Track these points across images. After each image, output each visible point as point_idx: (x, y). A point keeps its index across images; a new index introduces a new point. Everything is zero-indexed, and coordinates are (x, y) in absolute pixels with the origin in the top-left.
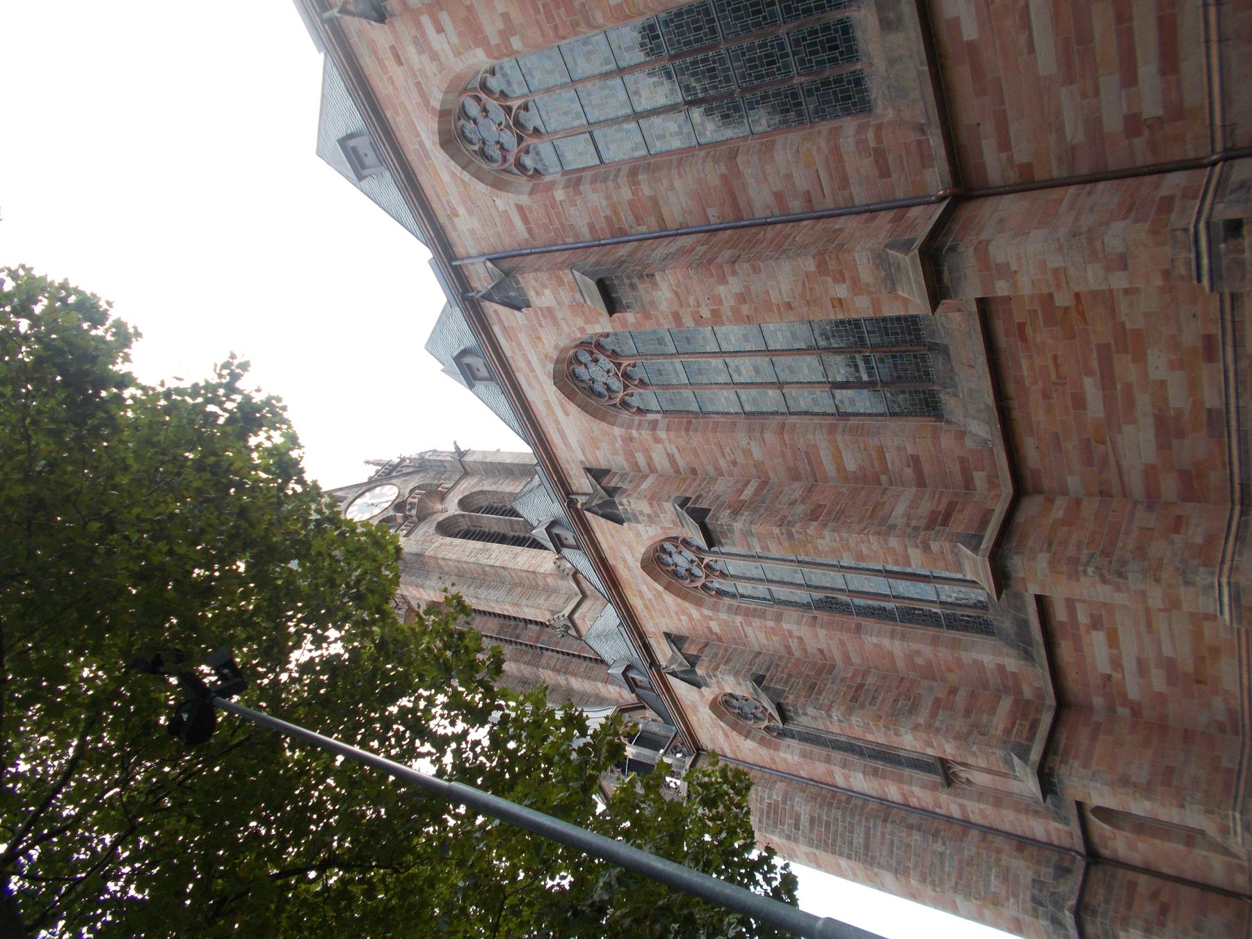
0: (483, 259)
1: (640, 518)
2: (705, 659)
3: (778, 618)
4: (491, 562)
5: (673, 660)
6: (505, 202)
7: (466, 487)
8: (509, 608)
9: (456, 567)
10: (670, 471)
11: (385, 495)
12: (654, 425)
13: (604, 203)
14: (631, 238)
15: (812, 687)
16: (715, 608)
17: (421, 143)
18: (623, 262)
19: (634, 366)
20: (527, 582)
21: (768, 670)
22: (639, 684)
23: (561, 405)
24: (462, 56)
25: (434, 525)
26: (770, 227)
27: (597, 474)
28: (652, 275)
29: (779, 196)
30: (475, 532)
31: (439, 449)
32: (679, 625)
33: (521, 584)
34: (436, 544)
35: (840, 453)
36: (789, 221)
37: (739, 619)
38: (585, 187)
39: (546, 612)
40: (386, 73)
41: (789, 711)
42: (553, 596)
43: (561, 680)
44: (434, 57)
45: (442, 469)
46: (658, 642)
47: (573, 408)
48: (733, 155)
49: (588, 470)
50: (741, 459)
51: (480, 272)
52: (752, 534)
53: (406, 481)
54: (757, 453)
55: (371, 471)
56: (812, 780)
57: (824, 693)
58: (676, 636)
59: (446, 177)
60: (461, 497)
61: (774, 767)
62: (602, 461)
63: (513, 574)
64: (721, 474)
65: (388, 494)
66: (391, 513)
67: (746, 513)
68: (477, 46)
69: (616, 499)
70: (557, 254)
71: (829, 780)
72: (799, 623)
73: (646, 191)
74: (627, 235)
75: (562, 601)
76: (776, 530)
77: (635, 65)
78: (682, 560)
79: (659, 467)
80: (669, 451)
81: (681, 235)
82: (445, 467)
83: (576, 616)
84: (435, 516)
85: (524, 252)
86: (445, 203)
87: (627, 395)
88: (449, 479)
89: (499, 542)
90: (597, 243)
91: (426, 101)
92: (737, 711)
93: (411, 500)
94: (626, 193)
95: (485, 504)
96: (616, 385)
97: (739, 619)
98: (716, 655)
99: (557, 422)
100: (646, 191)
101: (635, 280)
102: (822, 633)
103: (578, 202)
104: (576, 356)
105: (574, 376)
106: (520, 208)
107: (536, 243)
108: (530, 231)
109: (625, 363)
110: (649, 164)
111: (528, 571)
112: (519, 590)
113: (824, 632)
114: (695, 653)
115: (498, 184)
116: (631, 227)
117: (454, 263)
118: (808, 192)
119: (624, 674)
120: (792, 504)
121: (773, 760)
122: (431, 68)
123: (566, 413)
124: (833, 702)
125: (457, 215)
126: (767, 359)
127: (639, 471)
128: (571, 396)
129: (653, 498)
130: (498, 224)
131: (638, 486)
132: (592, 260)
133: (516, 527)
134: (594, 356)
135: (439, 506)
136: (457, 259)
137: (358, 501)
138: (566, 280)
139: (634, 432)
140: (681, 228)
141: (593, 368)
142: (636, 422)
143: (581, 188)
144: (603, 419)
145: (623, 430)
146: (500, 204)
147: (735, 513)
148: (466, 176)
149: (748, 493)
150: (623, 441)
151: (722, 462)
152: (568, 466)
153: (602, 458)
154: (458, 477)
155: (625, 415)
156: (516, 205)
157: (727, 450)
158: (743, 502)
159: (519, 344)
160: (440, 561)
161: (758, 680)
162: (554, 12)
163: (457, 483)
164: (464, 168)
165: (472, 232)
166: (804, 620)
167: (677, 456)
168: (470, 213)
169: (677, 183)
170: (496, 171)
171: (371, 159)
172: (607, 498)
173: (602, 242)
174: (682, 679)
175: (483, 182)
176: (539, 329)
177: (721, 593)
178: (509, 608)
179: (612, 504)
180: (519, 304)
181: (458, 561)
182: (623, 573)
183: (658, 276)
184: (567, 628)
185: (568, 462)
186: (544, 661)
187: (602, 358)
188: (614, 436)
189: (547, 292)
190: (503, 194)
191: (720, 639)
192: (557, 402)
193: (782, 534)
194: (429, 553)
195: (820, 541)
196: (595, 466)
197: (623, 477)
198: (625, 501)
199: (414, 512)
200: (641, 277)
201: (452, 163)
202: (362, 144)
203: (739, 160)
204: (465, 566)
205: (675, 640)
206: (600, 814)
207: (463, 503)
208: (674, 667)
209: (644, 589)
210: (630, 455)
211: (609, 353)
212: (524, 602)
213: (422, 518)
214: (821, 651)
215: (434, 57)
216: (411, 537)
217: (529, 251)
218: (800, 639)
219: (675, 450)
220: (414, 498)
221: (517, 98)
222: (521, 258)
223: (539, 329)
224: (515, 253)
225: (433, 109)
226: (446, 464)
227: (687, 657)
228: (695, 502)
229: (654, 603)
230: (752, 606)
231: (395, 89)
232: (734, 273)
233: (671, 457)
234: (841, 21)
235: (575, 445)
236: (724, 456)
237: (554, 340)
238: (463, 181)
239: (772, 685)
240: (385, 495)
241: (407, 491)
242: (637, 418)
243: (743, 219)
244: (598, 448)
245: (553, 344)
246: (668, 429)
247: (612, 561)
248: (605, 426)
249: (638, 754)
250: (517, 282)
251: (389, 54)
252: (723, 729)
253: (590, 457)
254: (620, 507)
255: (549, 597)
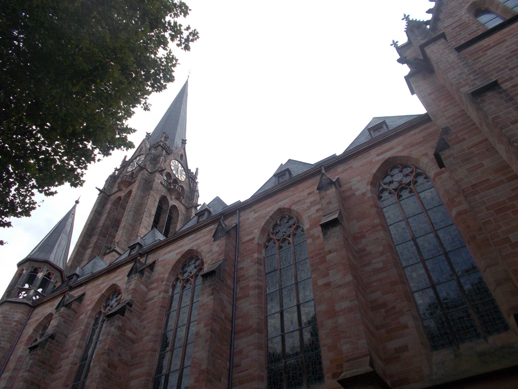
0: (237, 223)
1: (128, 285)
2: (69, 312)
3: (79, 347)
4: (144, 218)
5: (72, 296)
6: (257, 232)
7: (181, 208)
8: (123, 224)
9: (145, 203)
10: (147, 299)
11: (181, 176)
12: (166, 291)
13: (250, 274)
14: (235, 285)
15: (44, 363)
16: (90, 316)
17: (281, 201)
18: (222, 281)
19: (191, 284)
20: (134, 232)
21: (57, 341)
22: (70, 280)
23: (181, 252)
24: (308, 219)
25: (165, 195)
26: (229, 347)
27: (152, 266)
28: (213, 294)
29: (241, 352)
30: (161, 211)
31: (199, 198)
32: (87, 298)
33: (133, 230)
34: (155, 195)
35: (138, 378)
36: (230, 356)
37: (83, 328)
38: (256, 267)
39: (118, 240)
40: (306, 189)
41: (34, 351)
42: (126, 243)
43: (92, 245)
44: (309, 208)
45: (190, 199)
46: (82, 290)
47: (179, 256)
48: (259, 331)
49: (154, 262)
50: (145, 331)
51: (234, 221)
52: (108, 335)
53: (187, 184)
54: (146, 338)
55: (193, 171)
56: (8, 361)
57: (39, 368)
58: (83, 298)
59: (268, 209)
60: (177, 206)
61: (18, 343)
62: (157, 268)
63: (138, 226)
64: (141, 322)
65: (182, 177)
66: (173, 178)
67: (118, 333)
68: (310, 225)
69: (137, 274)
70: (234, 253)
71: (6, 370)
72: (75, 356)
73: (252, 292)
74: (237, 283)
75: (123, 246)
76: (107, 347)
77: (298, 290)
78: (191, 269)
79: (150, 293)
80: (155, 298)
81: (233, 307)
82: (191, 200)
83: (114, 253)
84: (169, 195)
85: (237, 240)
86: (260, 209)
87: (180, 280)
88: (186, 201)
89: (154, 221)
90: (236, 270)
91: (295, 203)
92: (47, 326)
93: (177, 186)
94: (252, 284)
95: (173, 216)
96: (185, 275)
97: (83, 328)
98: (70, 316)
99: (175, 250)
100: (252, 292)
101: (212, 287)
102: (68, 368)
103: (252, 263)
104: (198, 259)
105: (192, 258)
106: (253, 239)
107: (240, 244)
108: (245, 242)
109: (192, 280)
110: (262, 294)
111: (138, 233)
112: (131, 229)
113: (68, 369)
114: (72, 307)
115: (263, 230)
116: (240, 285)
117: (238, 211)
118: (240, 366)
119: (75, 274)
120: (119, 355)
121: (21, 342)
122: (305, 206)
123: (177, 254)
124: (33, 373)
125: (255, 213)
126: (182, 345)
127: (150, 284)
128: (184, 256)
129: (135, 290)
130: (249, 230)
131: (142, 283)
132: (227, 268)
133: (161, 228)
134: (197, 267)
135: (173, 197)
136: (239, 212)
137: (180, 165)
138: (220, 257)
139: (165, 283)
140: (235, 307)
141: (193, 266)
142: (169, 284)
143: (257, 265)
144: (172, 269)
145: (166, 278)
146: (256, 231)
147: (119, 328)
148: (268, 218)
149: (129, 334)
150: (163, 278)
151: (146, 322)
152: (157, 254)
153: (158, 268)
154: (186, 205)
155: (173, 279)
156: (255, 237)
157: (150, 325)
158: (125, 332)
159: (205, 235)
160: (148, 196)
161: (52, 337)
162: (318, 257)
163: (184, 205)
164: (271, 217)
165: (248, 219)
166: (76, 359)
167: (152, 301)
168: (255, 219)
169: (252, 306)
170: (269, 230)
171: (281, 180)
172: (139, 270)
173: (236, 273)
174: (61, 301)
175: (265, 224)
176: (210, 244)
177: (174, 287)
178: (123, 224)
179: (136, 272)
180: (215, 237)
181: (146, 204)
182: (112, 275)
183: (212, 297)
184: (110, 249)
185: (159, 254)
186: (101, 238)
187: (195, 270)
188: (165, 274)
189: (217, 249)
190: (259, 232)
191: (77, 318)
192: (182, 250)
193: (105, 350)
194: (152, 192)
195: (98, 368)
196: (156, 265)
197: (149, 278)
198: (136, 278)
199: (172, 187)
200: (213, 289)
201: (273, 212)
202: (287, 176)
203: (257, 334)
204: (144, 207)
205: (81, 298)
206: (310, 238)
207: (174, 207)
208: (67, 297)
209: (104, 285)
210: (156, 281)
211: (197, 273)
212: (125, 231)
213: (169, 190)
214: (61, 367)
215: (309, 208)
216: (161, 185)
217: (237, 241)
218: (68, 357)
219: (155, 300)
220: (178, 187)
221: (293, 240)
222: (235, 238)
223: (210, 244)
224: (238, 236)
225: (291, 206)
226: (192, 201)
227: (71, 303)
228: (129, 310)
229: (98, 289)
230: (87, 334)
231: (300, 192)
232: (207, 330)
233: (152, 299)
234: (302, 382)
235: (165, 257)
236: (148, 323)
237: (204, 249)
238: (266, 216)
239: (48, 343)
240: (181, 176)
241: (182, 185)
242: (171, 284)
243: (234, 335)
244: (162, 267)
245: (203, 250)
246: (163, 298)
247: (118, 271)
248: (169, 270)
249: (38, 279)
250: (223, 236)
251: (312, 190)
252: (40, 319)
253: (160, 263)
254: (134, 276)
255: (126, 241)
